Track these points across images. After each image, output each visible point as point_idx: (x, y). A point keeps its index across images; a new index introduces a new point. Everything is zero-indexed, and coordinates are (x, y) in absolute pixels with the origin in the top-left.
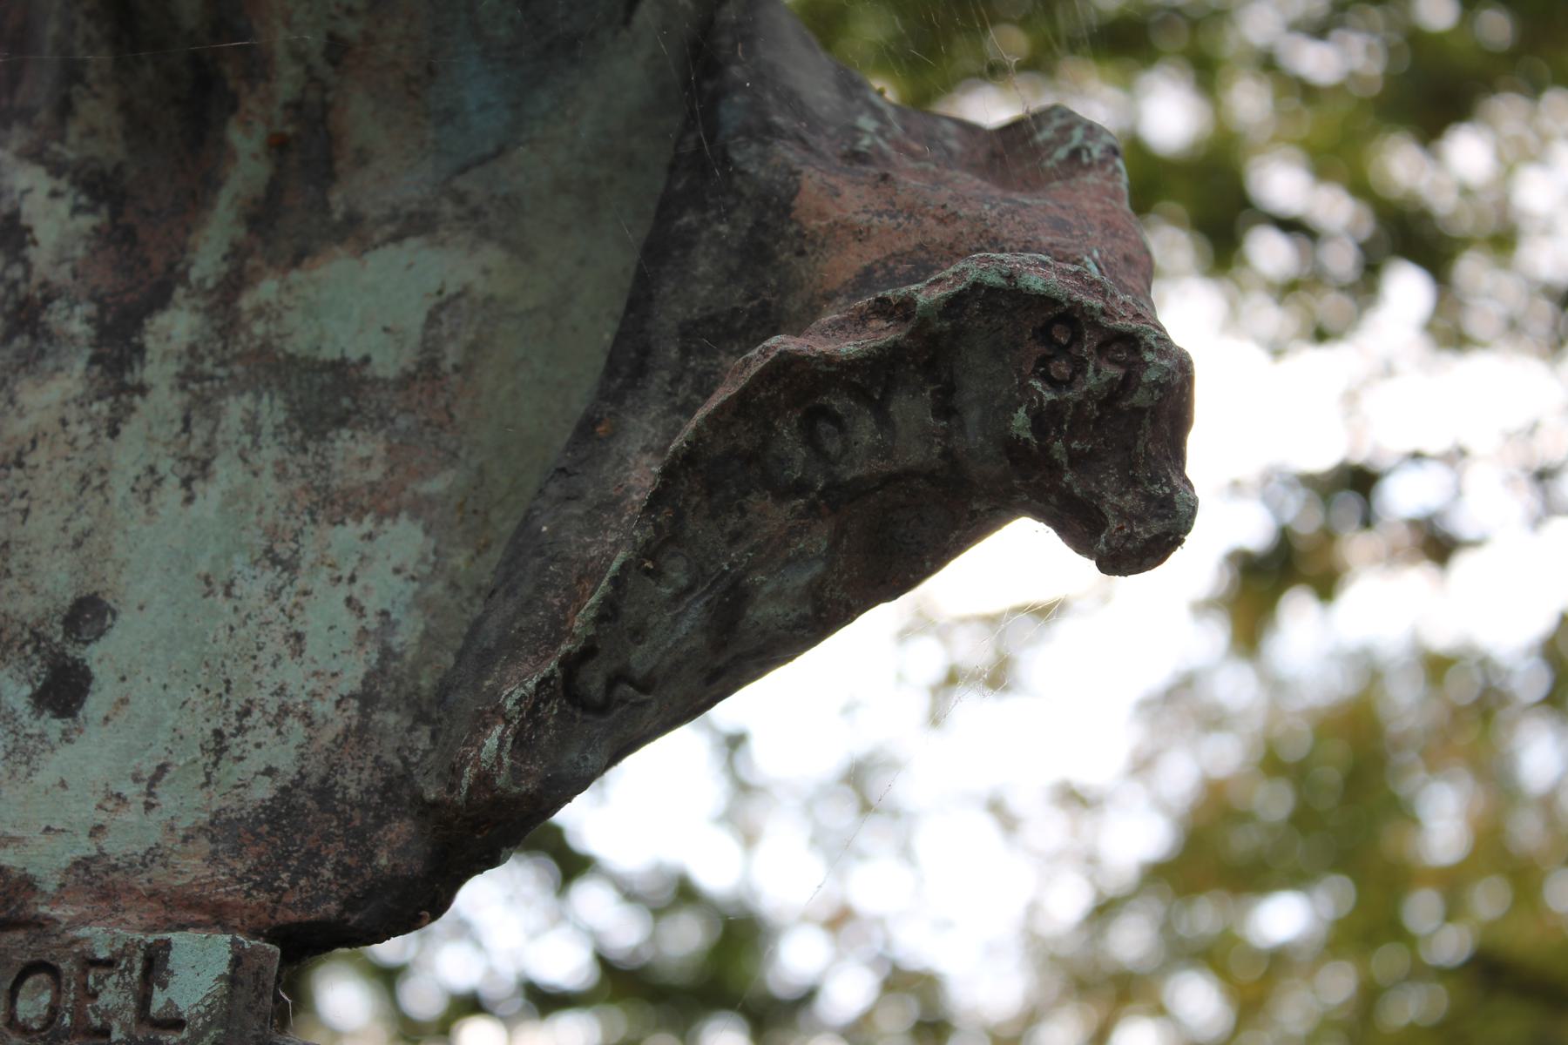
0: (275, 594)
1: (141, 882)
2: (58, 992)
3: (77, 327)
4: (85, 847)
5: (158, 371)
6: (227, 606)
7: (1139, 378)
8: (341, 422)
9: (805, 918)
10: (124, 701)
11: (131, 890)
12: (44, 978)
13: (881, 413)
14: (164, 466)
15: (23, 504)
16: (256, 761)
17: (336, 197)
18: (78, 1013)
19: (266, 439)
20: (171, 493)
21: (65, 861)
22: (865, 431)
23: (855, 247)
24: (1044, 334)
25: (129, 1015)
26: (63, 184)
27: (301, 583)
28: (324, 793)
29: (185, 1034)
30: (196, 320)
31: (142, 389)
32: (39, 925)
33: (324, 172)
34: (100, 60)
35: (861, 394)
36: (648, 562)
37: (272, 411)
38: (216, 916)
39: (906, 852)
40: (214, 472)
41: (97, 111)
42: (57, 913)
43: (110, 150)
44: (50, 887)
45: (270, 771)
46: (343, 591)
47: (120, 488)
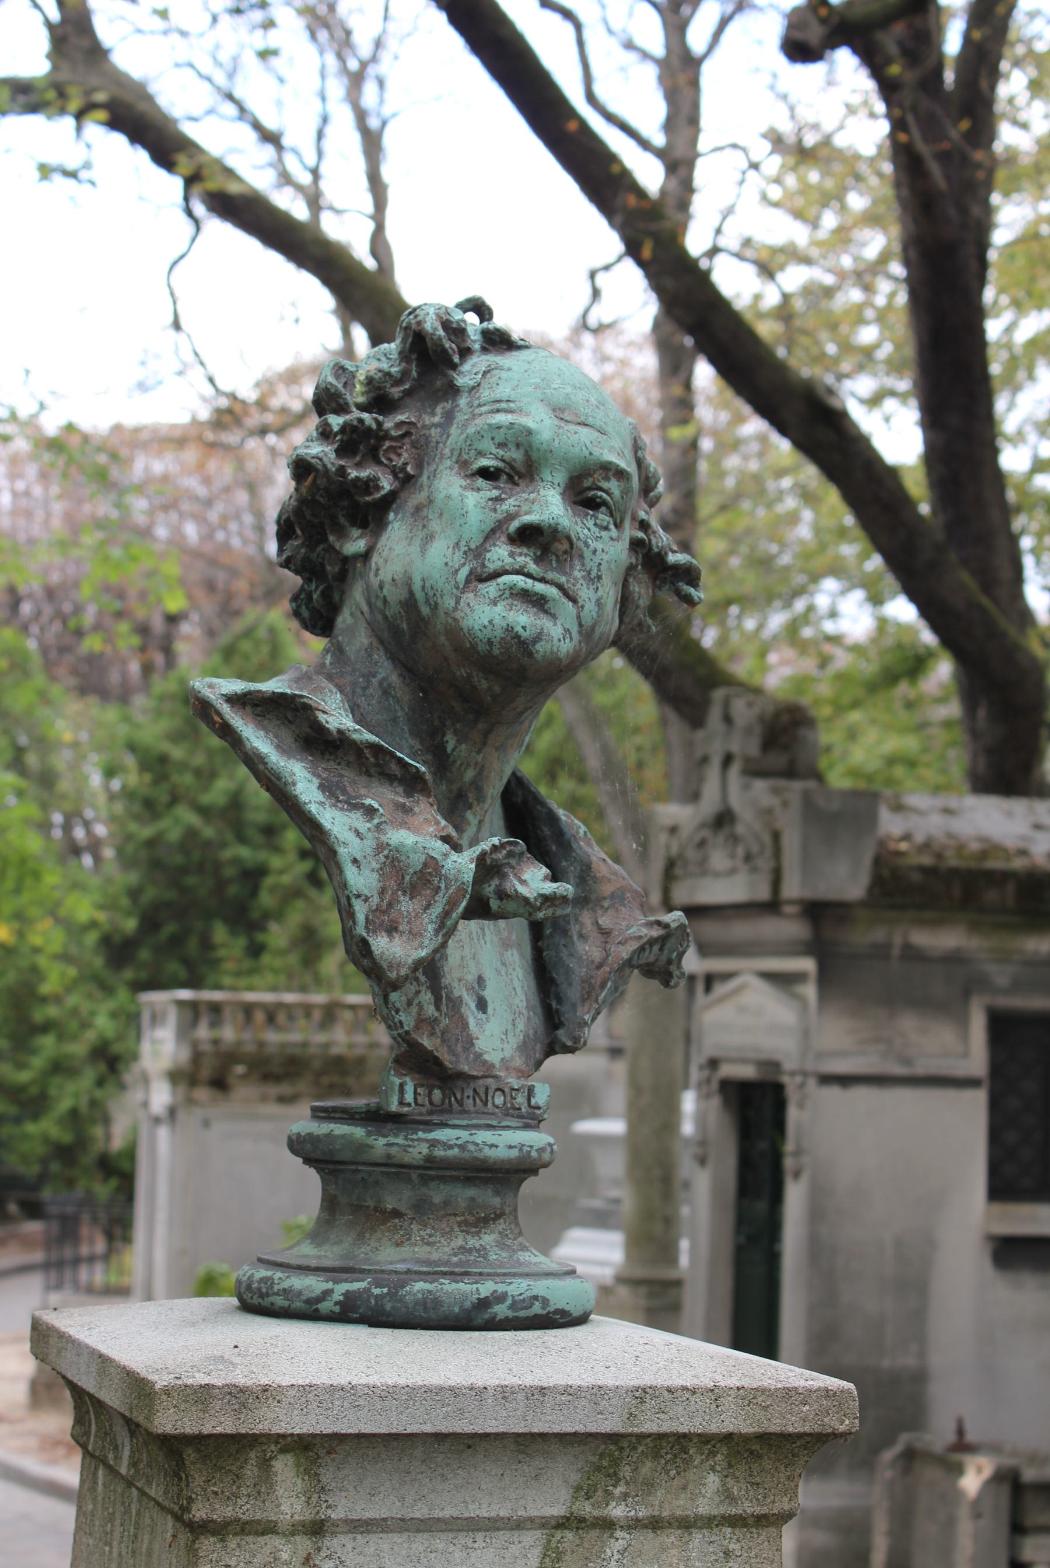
2: (505, 1097)
7: (535, 1159)
18: (512, 1104)
25: (526, 1105)
32: (495, 1077)
39: (624, 319)
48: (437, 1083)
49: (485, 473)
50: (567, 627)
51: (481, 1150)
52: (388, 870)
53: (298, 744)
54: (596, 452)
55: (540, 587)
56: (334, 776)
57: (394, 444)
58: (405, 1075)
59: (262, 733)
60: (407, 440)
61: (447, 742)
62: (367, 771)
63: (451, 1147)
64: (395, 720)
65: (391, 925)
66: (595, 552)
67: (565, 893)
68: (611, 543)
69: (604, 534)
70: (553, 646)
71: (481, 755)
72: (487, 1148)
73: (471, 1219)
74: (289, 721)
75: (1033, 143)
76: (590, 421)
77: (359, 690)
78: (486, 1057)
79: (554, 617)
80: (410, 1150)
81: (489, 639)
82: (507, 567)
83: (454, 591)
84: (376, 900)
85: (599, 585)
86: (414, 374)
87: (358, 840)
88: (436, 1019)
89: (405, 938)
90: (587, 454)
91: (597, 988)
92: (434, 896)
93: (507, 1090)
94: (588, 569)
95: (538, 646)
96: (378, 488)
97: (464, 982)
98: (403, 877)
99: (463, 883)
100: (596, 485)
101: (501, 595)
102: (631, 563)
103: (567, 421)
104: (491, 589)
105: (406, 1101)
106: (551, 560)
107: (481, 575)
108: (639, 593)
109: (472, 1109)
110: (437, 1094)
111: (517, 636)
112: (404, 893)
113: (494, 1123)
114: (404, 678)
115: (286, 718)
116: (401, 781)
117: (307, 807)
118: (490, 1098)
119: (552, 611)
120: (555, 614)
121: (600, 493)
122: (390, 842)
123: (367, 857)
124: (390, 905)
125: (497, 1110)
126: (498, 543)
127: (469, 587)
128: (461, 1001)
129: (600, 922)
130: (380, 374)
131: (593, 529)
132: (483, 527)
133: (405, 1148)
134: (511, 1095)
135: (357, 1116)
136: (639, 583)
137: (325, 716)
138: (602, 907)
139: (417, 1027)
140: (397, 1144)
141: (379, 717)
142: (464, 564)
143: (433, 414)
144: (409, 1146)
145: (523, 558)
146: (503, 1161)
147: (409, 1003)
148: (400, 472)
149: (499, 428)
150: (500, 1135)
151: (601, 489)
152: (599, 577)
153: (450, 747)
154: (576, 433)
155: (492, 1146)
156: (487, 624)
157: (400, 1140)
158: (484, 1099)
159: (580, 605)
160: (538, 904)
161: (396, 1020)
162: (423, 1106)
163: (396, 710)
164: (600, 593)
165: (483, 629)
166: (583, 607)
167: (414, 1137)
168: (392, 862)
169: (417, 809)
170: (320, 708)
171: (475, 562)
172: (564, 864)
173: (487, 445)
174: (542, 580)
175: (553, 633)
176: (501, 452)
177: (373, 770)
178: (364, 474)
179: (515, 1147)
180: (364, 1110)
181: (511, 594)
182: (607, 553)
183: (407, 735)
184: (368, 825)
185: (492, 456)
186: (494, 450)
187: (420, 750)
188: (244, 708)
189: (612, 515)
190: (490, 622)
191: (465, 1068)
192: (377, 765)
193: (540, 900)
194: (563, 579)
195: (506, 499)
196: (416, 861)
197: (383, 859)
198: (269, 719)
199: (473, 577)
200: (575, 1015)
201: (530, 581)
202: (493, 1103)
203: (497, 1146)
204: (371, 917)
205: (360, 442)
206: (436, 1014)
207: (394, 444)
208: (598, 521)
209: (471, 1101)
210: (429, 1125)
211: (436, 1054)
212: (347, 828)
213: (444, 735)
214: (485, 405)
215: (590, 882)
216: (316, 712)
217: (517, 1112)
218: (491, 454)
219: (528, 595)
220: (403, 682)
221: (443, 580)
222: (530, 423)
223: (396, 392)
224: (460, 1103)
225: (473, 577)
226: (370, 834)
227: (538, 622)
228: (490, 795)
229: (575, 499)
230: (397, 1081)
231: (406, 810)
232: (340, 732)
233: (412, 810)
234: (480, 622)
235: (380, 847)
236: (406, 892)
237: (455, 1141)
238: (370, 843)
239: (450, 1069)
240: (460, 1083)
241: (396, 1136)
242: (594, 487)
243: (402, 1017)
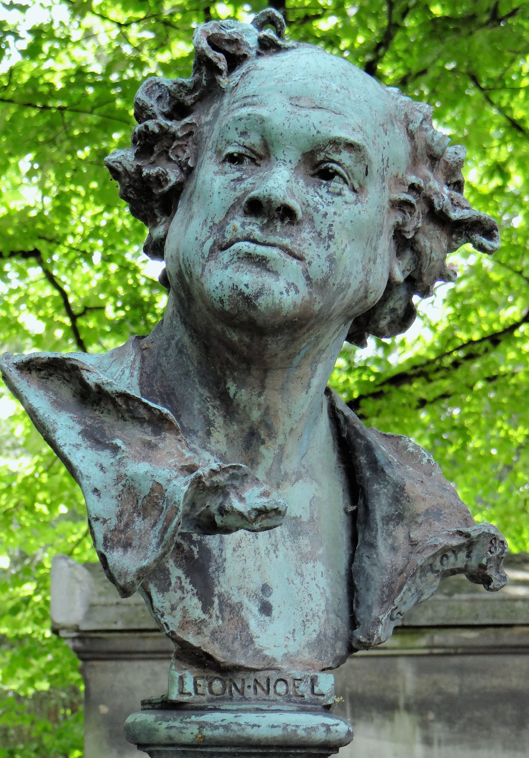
6: (294, 587)
10: (281, 612)
11: (296, 661)
15: (243, 558)
16: (311, 629)
19: (287, 540)
20: (272, 555)
21: (282, 653)
23: (423, 503)
25: (309, 691)
28: (325, 635)
29: (325, 697)
32: (278, 670)
35: (454, 552)
42: (283, 667)
44: (279, 660)
45: (314, 631)
48: (218, 675)
49: (232, 159)
50: (290, 281)
51: (243, 730)
52: (125, 496)
53: (75, 399)
54: (323, 130)
55: (261, 250)
56: (97, 423)
57: (180, 143)
58: (185, 669)
59: (42, 392)
60: (190, 139)
61: (229, 388)
62: (123, 416)
63: (217, 728)
64: (187, 374)
65: (127, 542)
66: (325, 215)
67: (276, 507)
68: (345, 206)
69: (336, 199)
70: (273, 298)
71: (263, 398)
72: (249, 728)
74: (68, 381)
76: (325, 104)
77: (162, 352)
78: (266, 652)
79: (276, 273)
80: (184, 731)
81: (220, 298)
82: (239, 236)
83: (201, 260)
84: (114, 521)
85: (330, 243)
86: (204, 83)
87: (101, 473)
88: (203, 621)
89: (135, 551)
90: (315, 132)
91: (396, 592)
92: (159, 516)
94: (318, 230)
95: (260, 300)
96: (167, 181)
97: (245, 590)
98: (137, 501)
99: (175, 503)
100: (328, 158)
101: (231, 260)
102: (398, 222)
103: (301, 107)
104: (225, 256)
105: (186, 691)
106: (276, 226)
107: (221, 245)
108: (431, 248)
109: (253, 696)
110: (217, 685)
111: (241, 293)
112: (139, 514)
113: (264, 707)
114: (193, 338)
115: (65, 379)
116: (150, 422)
117: (61, 449)
118: (271, 687)
119: (274, 269)
120: (277, 272)
121: (331, 165)
122: (128, 473)
123: (108, 486)
124: (127, 525)
125: (278, 698)
126: (236, 216)
127: (212, 256)
128: (241, 606)
129: (412, 536)
130: (175, 86)
131: (326, 196)
132: (224, 204)
133: (181, 730)
134: (294, 685)
135: (156, 706)
136: (430, 239)
137: (88, 374)
138: (416, 522)
139: (182, 627)
140: (175, 727)
141: (176, 372)
142: (210, 237)
143: (207, 114)
144: (184, 728)
145: (251, 227)
146: (266, 739)
147: (173, 608)
148: (184, 166)
149: (240, 119)
150: (264, 717)
151: (333, 161)
152: (331, 237)
153: (232, 392)
154: (307, 116)
155: (254, 726)
156: (218, 285)
157: (177, 724)
158: (265, 688)
159: (307, 261)
160: (253, 517)
161: (162, 622)
162: (203, 695)
163: (188, 366)
164: (331, 250)
165: (216, 290)
166: (310, 263)
167: (188, 720)
168: (129, 489)
169: (161, 445)
170: (85, 367)
171: (218, 234)
172: (376, 486)
173: (234, 136)
174: (264, 244)
175: (273, 287)
176: (242, 140)
177: (126, 415)
178: (153, 171)
179: (278, 726)
180: (160, 701)
181: (239, 258)
182: (340, 215)
183: (197, 386)
184: (112, 460)
185: (236, 144)
186: (237, 139)
187: (209, 397)
188: (30, 373)
189: (346, 182)
190: (221, 283)
191: (242, 662)
192: (129, 411)
193: (254, 514)
194: (286, 241)
195: (247, 179)
196: (145, 487)
197: (121, 488)
198: (52, 380)
199: (216, 247)
200: (370, 615)
201: (253, 246)
202: (275, 692)
203: (259, 726)
204: (109, 536)
205: (154, 145)
206: (204, 616)
207: (180, 143)
208: (330, 189)
209: (252, 690)
210: (201, 709)
211: (205, 650)
212: (93, 464)
213: (225, 383)
214: (237, 101)
215: (404, 502)
216: (82, 371)
217: (300, 699)
218: (235, 142)
219: (252, 258)
220: (192, 342)
221: (194, 252)
222: (263, 112)
223: (189, 100)
224: (241, 692)
225: (216, 247)
226: (112, 468)
227: (260, 279)
228: (280, 431)
229: (312, 172)
230: (177, 675)
231: (150, 446)
232: (98, 386)
233: (156, 445)
234: (214, 284)
235: (119, 478)
236: (140, 513)
237: (220, 723)
238: (111, 475)
239: (223, 663)
240: (241, 675)
241: (175, 720)
242: (327, 160)
243: (167, 619)
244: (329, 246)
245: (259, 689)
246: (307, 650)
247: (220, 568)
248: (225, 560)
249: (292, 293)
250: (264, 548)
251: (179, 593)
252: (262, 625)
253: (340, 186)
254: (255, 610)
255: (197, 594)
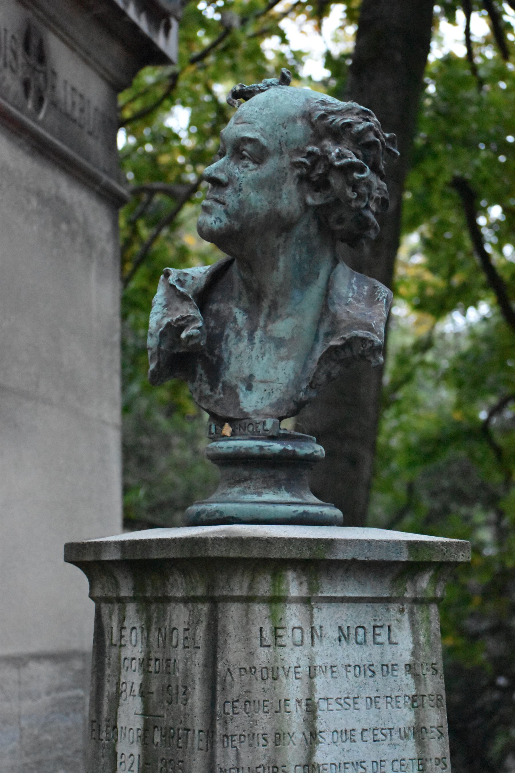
0: (275, 373)
1: (262, 412)
3: (246, 334)
4: (255, 408)
5: (257, 341)
8: (282, 346)
9: (478, 313)
12: (251, 425)
13: (344, 351)
14: (259, 355)
17: (278, 311)
20: (260, 359)
22: (343, 353)
24: (362, 341)
26: (241, 311)
27: (278, 371)
30: (261, 332)
31: (255, 344)
32: (250, 419)
33: (276, 309)
34: (244, 292)
36: (318, 370)
37: (272, 346)
38: (272, 416)
40: (322, 57)
41: (245, 299)
43: (247, 305)
44: (251, 414)
46: (284, 371)
47: (254, 358)
50: (217, 217)
66: (238, 179)
73: (232, 481)
75: (511, 52)
93: (254, 424)
194: (217, 196)
209: (238, 430)
244: (239, 195)
245: (241, 429)
246: (269, 408)
247: (227, 368)
248: (230, 364)
249: (218, 223)
250: (255, 356)
251: (199, 382)
252: (246, 396)
253: (246, 162)
254: (244, 388)
255: (209, 382)
